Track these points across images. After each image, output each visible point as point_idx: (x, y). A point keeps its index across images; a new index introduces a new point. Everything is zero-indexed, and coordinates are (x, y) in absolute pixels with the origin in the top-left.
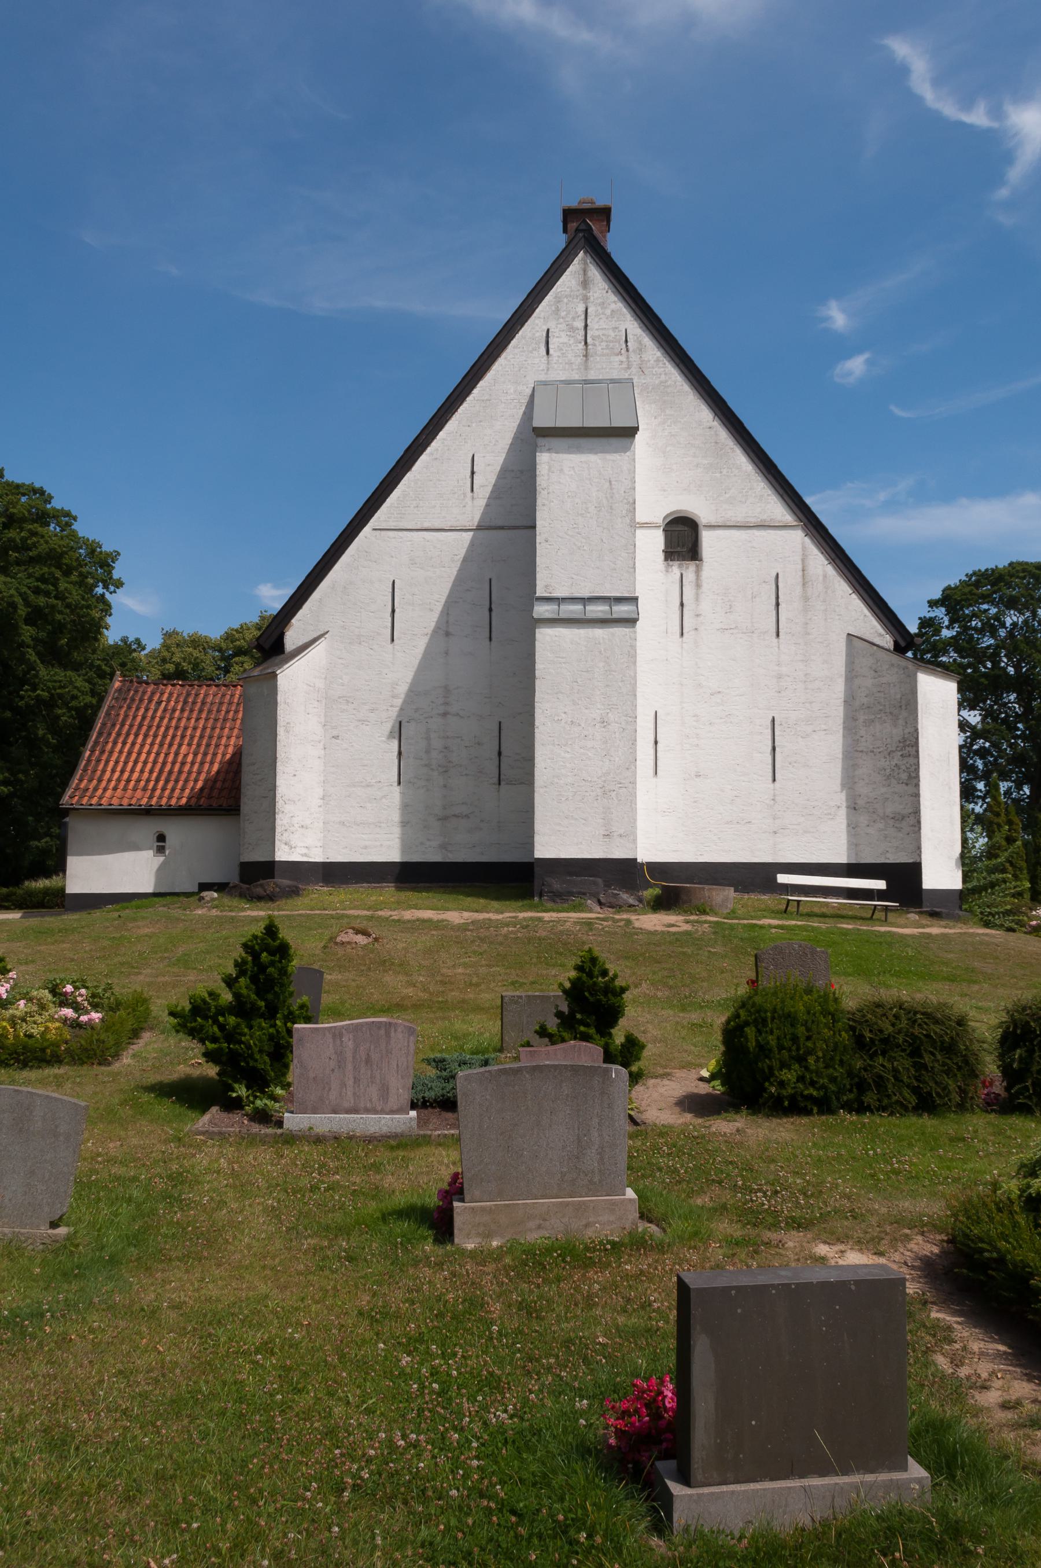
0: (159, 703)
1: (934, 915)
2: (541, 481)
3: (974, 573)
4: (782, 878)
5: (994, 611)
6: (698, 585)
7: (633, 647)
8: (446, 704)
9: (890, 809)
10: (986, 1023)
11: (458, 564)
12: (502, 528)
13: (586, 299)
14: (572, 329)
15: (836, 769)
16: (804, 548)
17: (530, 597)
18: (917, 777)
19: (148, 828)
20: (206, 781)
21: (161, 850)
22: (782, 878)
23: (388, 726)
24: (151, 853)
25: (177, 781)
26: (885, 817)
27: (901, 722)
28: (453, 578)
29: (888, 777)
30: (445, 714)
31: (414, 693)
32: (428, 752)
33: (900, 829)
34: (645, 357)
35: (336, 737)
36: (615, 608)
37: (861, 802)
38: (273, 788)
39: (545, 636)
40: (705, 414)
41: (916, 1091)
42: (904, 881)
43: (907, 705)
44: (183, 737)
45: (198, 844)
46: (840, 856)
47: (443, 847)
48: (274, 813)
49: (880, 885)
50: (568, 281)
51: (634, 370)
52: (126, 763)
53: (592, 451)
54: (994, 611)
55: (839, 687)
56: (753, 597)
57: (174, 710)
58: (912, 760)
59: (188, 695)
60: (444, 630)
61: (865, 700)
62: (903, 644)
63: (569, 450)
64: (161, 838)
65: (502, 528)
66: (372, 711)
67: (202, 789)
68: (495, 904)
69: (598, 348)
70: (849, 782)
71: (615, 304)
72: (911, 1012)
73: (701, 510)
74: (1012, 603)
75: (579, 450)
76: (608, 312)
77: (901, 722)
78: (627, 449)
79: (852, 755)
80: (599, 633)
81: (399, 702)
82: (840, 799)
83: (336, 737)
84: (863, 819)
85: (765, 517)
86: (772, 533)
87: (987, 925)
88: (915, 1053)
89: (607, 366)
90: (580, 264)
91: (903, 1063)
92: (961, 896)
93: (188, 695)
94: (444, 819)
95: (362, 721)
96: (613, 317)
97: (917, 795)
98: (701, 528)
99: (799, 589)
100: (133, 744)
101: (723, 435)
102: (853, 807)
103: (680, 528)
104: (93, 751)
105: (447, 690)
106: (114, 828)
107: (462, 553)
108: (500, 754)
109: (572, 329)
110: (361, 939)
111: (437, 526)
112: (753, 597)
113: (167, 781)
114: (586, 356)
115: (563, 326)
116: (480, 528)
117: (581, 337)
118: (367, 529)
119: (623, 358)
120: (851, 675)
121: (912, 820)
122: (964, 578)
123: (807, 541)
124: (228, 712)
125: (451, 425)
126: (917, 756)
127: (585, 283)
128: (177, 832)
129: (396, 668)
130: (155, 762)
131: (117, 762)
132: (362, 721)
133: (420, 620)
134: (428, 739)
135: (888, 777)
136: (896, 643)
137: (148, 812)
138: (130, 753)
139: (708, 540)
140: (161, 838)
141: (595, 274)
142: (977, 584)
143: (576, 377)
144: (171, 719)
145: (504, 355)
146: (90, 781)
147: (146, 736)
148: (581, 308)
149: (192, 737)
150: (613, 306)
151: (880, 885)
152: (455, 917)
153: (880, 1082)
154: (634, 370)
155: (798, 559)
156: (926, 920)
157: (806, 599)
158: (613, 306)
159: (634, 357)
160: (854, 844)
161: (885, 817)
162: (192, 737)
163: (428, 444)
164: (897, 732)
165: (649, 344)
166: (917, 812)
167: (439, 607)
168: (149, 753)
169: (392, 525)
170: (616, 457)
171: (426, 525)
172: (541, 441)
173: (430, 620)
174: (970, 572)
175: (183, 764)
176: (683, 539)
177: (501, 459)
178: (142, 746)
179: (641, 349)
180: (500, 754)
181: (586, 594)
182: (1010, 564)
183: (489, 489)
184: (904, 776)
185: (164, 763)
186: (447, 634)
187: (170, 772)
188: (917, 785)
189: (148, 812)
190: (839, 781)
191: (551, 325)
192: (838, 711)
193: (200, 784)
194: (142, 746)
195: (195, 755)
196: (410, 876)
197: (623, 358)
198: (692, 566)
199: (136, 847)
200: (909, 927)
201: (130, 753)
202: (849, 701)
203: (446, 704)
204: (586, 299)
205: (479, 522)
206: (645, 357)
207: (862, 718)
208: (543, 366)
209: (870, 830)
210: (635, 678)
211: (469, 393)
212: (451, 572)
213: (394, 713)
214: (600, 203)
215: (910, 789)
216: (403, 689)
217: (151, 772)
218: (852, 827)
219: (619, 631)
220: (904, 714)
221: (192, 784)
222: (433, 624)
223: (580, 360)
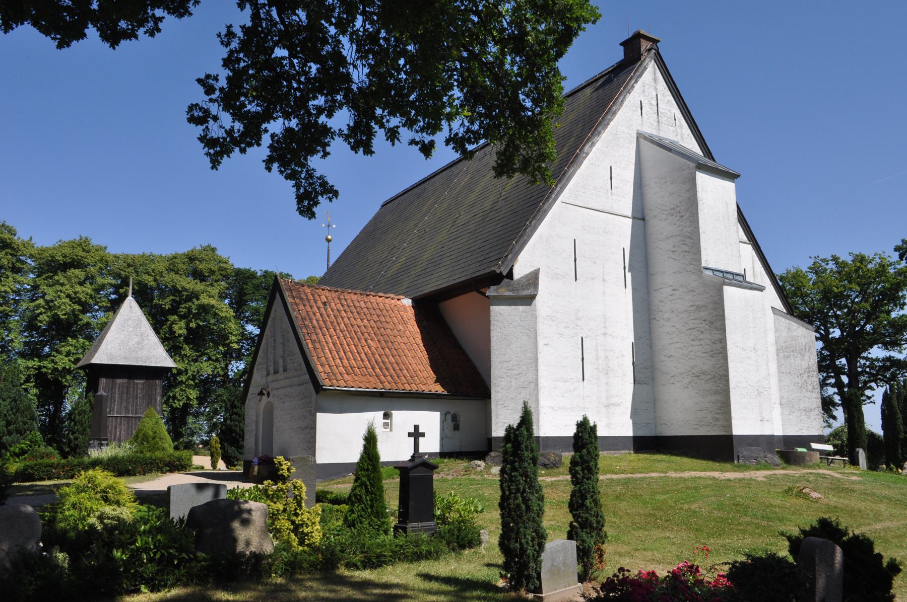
9: (802, 405)
13: (656, 89)
27: (806, 358)
30: (605, 334)
69: (663, 119)
77: (806, 358)
127: (655, 80)
154: (679, 137)
189: (381, 395)
203: (605, 327)
204: (656, 89)
208: (640, 122)
223: (656, 124)
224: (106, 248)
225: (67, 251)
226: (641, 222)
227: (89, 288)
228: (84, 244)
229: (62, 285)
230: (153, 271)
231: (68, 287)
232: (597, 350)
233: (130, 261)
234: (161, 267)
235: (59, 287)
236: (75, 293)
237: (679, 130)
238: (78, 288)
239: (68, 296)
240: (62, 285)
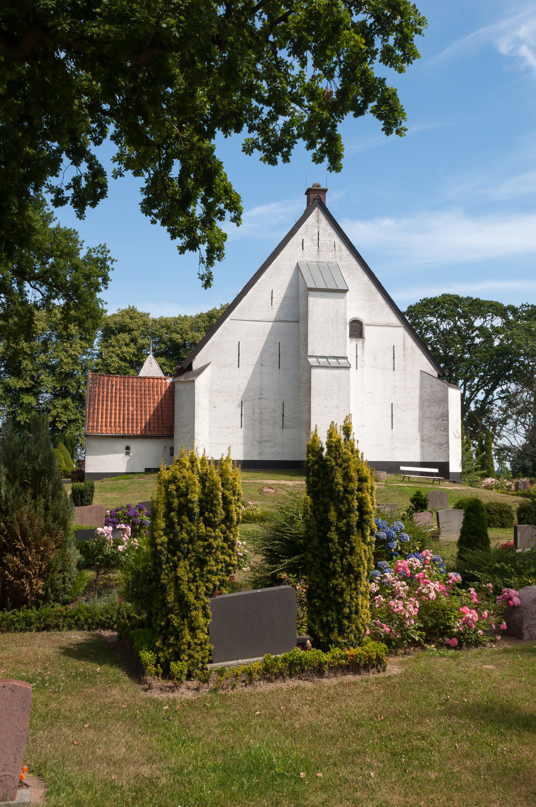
0: (112, 386)
1: (454, 482)
2: (310, 309)
3: (424, 299)
4: (402, 468)
5: (435, 321)
6: (363, 349)
7: (349, 378)
8: (261, 394)
9: (437, 441)
10: (515, 508)
11: (266, 336)
12: (284, 321)
13: (318, 227)
14: (313, 240)
15: (416, 424)
16: (404, 336)
17: (306, 356)
18: (448, 429)
19: (121, 445)
20: (146, 423)
21: (127, 454)
22: (402, 468)
23: (238, 402)
24: (123, 455)
25: (132, 423)
26: (435, 444)
27: (442, 407)
28: (264, 342)
29: (436, 428)
30: (260, 399)
31: (248, 389)
32: (253, 414)
33: (441, 449)
34: (342, 253)
35: (215, 407)
36: (340, 361)
37: (425, 438)
38: (193, 429)
39: (315, 372)
40: (366, 278)
41: (501, 522)
42: (444, 467)
43: (444, 400)
44: (128, 402)
45: (146, 453)
46: (417, 459)
47: (260, 454)
48: (194, 440)
49: (436, 470)
50: (311, 219)
51: (338, 258)
52: (106, 414)
53: (330, 297)
54: (435, 321)
55: (417, 392)
56: (385, 354)
57: (120, 390)
58: (446, 422)
59: (124, 382)
60: (261, 363)
61: (427, 397)
62: (441, 375)
63: (321, 297)
64: (128, 448)
65: (284, 321)
66: (230, 396)
67: (145, 427)
68: (288, 477)
69: (323, 248)
70: (421, 429)
71: (330, 230)
72: (500, 504)
73: (364, 318)
74: (443, 317)
75: (325, 297)
76: (327, 234)
77: (442, 407)
78: (343, 298)
79: (423, 418)
80: (336, 372)
81: (241, 393)
82: (418, 436)
83: (215, 407)
84: (426, 444)
85: (389, 322)
86: (392, 328)
87: (471, 486)
88: (500, 514)
89: (327, 257)
90: (316, 212)
91: (498, 516)
92: (462, 473)
93: (124, 382)
94: (260, 442)
95: (226, 401)
96: (329, 236)
97: (448, 436)
98: (364, 325)
99: (402, 352)
100: (107, 405)
101: (373, 287)
102: (422, 440)
103: (355, 324)
104: (89, 408)
105: (261, 388)
106: (107, 444)
107: (268, 331)
108: (283, 415)
109: (313, 240)
110: (271, 490)
111: (257, 319)
112: (385, 354)
113: (128, 423)
114: (318, 251)
115: (309, 238)
116: (275, 321)
117: (316, 243)
118: (228, 320)
119: (333, 253)
120: (422, 387)
121: (446, 445)
122: (419, 302)
123: (406, 332)
124: (145, 391)
125: (263, 277)
126: (448, 421)
127: (318, 221)
128: (136, 446)
129: (241, 378)
130: (120, 414)
131: (102, 414)
132: (226, 401)
133: (251, 358)
134: (253, 409)
135: (436, 428)
136: (439, 375)
137: (123, 437)
138: (107, 410)
139: (367, 331)
140: (128, 448)
141: (322, 217)
142: (425, 305)
143: (315, 260)
144: (120, 394)
145: (285, 249)
146: (93, 422)
147: (111, 401)
148: (316, 231)
149: (133, 402)
150: (329, 231)
151: (436, 470)
152: (290, 483)
153: (493, 520)
154: (338, 258)
155: (402, 339)
156: (452, 484)
157: (405, 356)
158: (329, 231)
159: (338, 253)
160: (423, 455)
161: (435, 444)
162: (133, 402)
163: (253, 285)
164: (440, 411)
165: (343, 247)
166: (448, 442)
167: (258, 354)
168: (115, 410)
169: (238, 318)
170: (339, 300)
171: (253, 319)
172: (310, 293)
173: (255, 359)
174: (422, 299)
175: (133, 415)
176: (357, 329)
177: (284, 292)
178: (111, 406)
179: (340, 250)
180: (283, 415)
181: (327, 355)
182: (443, 295)
183: (279, 305)
184: (443, 428)
185: (124, 415)
186: (262, 365)
187: (128, 419)
188: (448, 432)
189: (123, 437)
190: (417, 429)
191: (304, 237)
192: (417, 401)
193: (143, 425)
194: (111, 406)
195: (137, 411)
196: (247, 465)
197: (333, 253)
198: (361, 340)
199: (117, 452)
200: (447, 486)
201: (107, 410)
202: (421, 397)
203: (261, 394)
204: (318, 227)
205: (276, 318)
206: (342, 253)
207: (426, 404)
208: (301, 255)
209: (429, 449)
210: (349, 390)
211: (270, 264)
212: (263, 339)
213: (239, 398)
214: (323, 187)
215: (445, 433)
216: (243, 387)
217: (119, 418)
218: (422, 447)
219: (343, 371)
220: (443, 404)
221: (139, 425)
222: (256, 361)
223: (316, 253)
224: (149, 314)
225: (118, 319)
226: (296, 324)
227: (132, 349)
228: (131, 313)
229: (114, 347)
230: (181, 329)
231: (117, 348)
232: (253, 409)
233: (163, 323)
234: (186, 326)
235: (111, 349)
236: (123, 353)
237: (338, 253)
238: (125, 349)
239: (118, 355)
240: (114, 347)
